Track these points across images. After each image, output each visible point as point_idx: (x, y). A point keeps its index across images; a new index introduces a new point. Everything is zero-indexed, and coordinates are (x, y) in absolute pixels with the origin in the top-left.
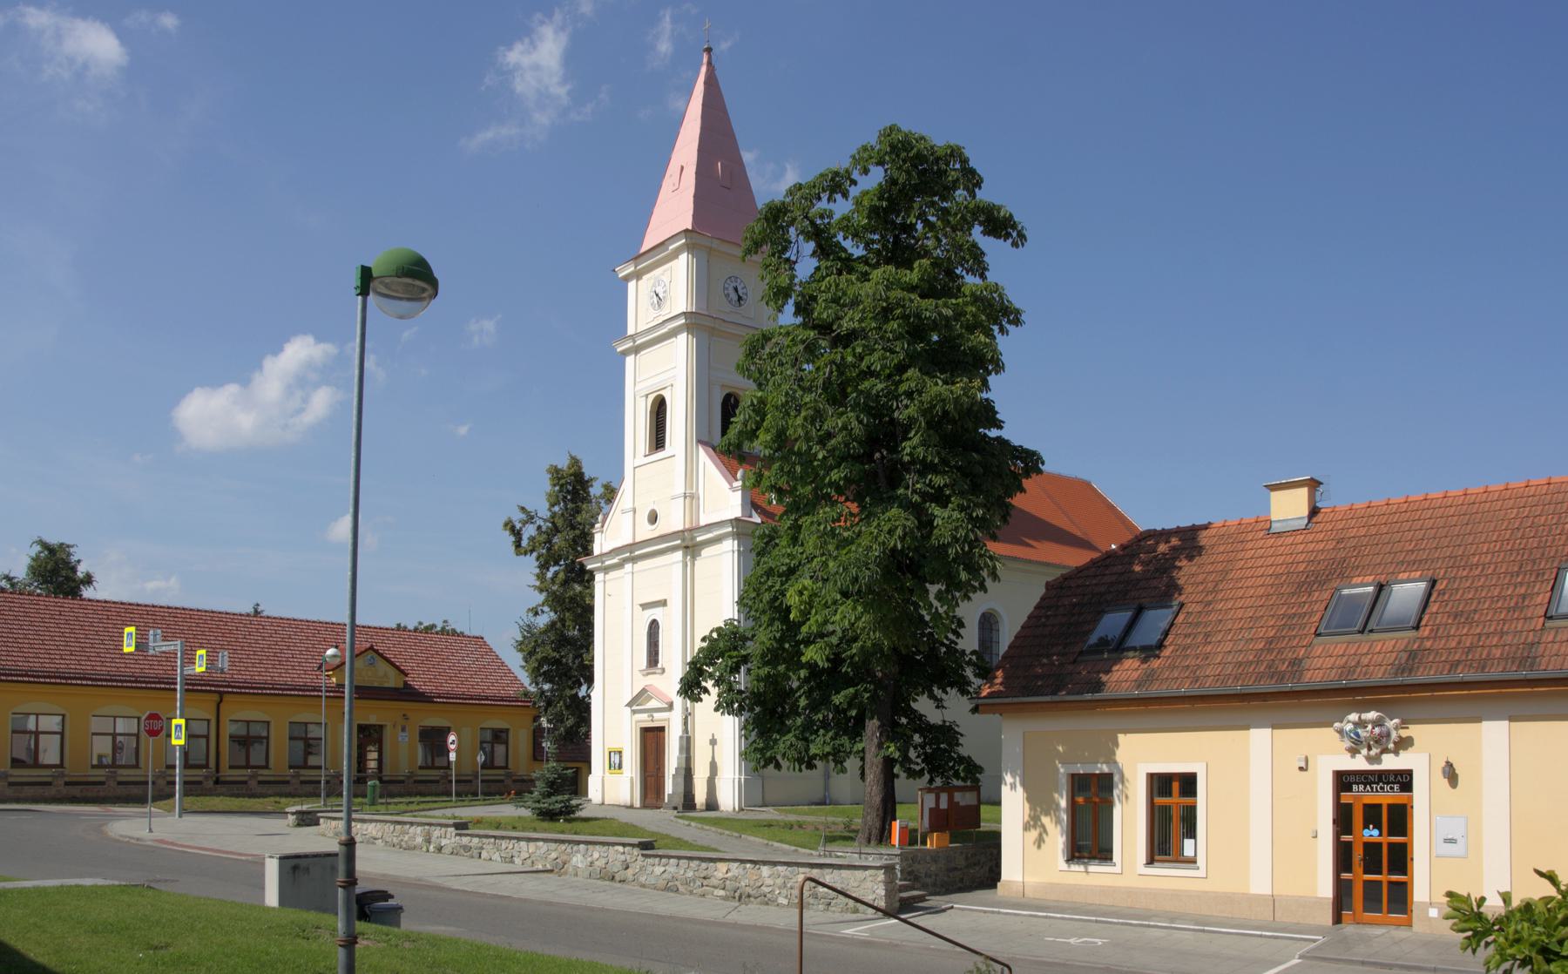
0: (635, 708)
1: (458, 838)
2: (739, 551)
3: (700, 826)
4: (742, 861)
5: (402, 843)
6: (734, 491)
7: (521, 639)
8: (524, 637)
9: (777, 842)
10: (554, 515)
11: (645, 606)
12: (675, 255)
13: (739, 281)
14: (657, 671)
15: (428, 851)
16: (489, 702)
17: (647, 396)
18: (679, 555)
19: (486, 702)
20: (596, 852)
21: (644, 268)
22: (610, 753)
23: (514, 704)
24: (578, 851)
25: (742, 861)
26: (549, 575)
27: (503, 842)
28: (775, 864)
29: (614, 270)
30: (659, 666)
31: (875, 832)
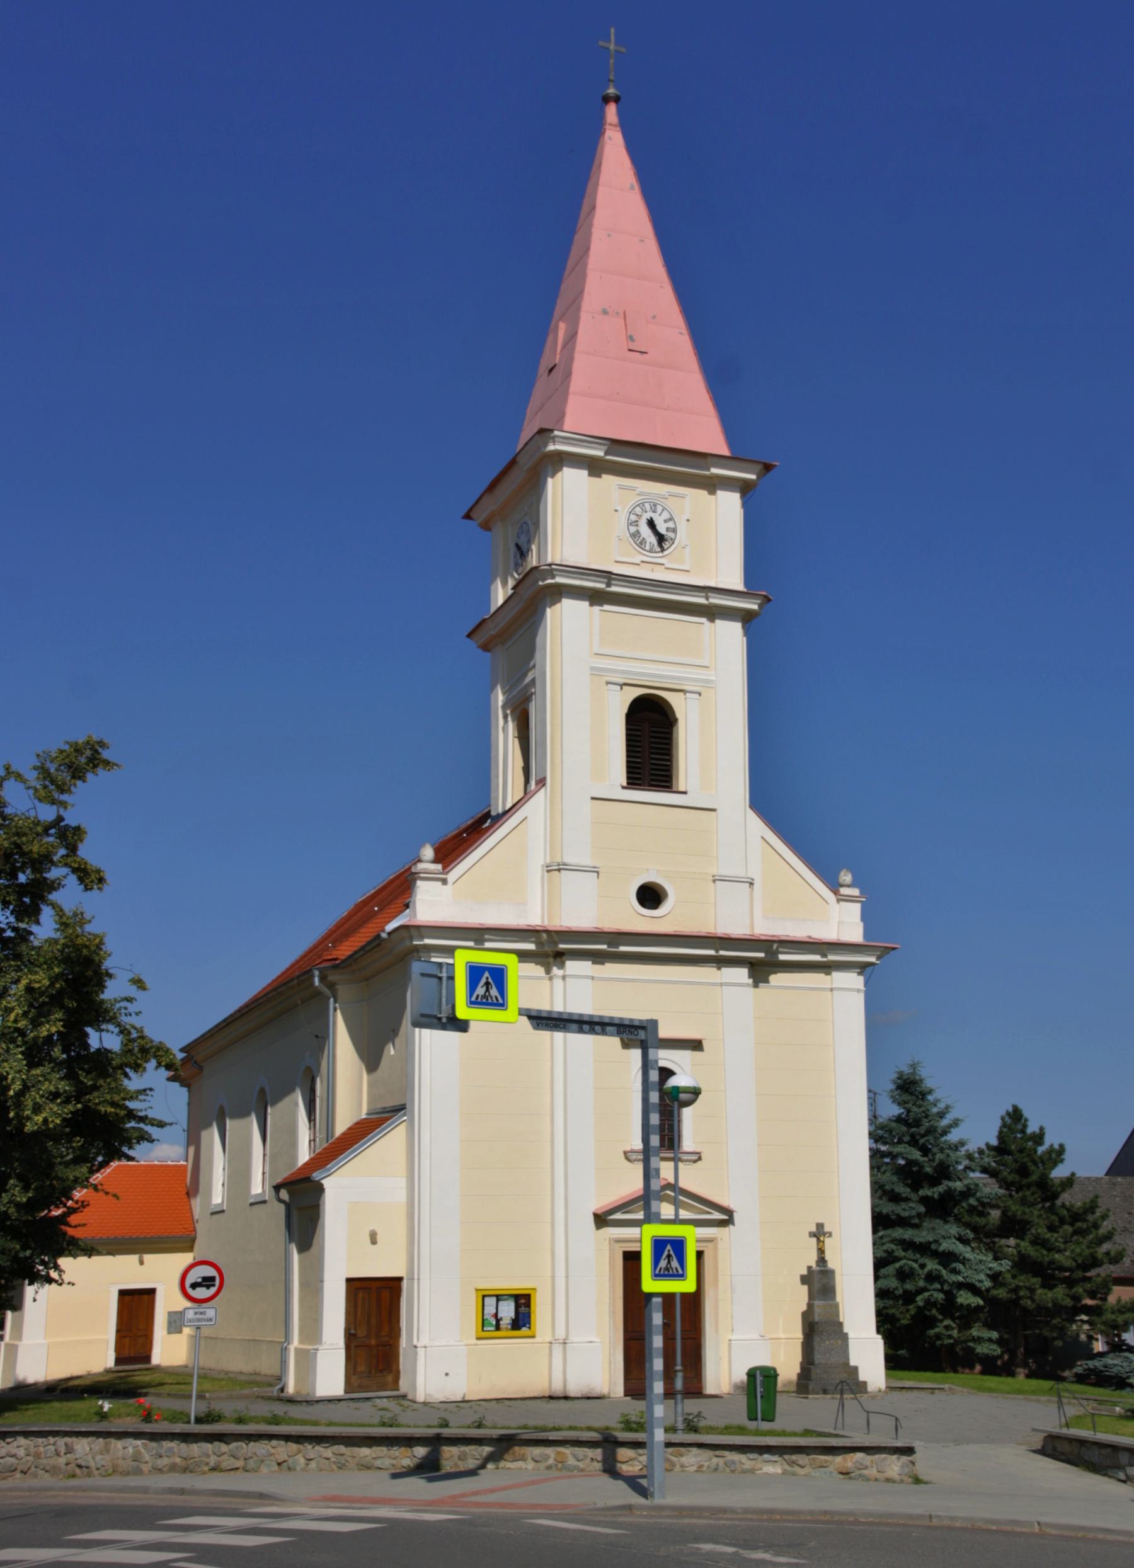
13: (659, 509)
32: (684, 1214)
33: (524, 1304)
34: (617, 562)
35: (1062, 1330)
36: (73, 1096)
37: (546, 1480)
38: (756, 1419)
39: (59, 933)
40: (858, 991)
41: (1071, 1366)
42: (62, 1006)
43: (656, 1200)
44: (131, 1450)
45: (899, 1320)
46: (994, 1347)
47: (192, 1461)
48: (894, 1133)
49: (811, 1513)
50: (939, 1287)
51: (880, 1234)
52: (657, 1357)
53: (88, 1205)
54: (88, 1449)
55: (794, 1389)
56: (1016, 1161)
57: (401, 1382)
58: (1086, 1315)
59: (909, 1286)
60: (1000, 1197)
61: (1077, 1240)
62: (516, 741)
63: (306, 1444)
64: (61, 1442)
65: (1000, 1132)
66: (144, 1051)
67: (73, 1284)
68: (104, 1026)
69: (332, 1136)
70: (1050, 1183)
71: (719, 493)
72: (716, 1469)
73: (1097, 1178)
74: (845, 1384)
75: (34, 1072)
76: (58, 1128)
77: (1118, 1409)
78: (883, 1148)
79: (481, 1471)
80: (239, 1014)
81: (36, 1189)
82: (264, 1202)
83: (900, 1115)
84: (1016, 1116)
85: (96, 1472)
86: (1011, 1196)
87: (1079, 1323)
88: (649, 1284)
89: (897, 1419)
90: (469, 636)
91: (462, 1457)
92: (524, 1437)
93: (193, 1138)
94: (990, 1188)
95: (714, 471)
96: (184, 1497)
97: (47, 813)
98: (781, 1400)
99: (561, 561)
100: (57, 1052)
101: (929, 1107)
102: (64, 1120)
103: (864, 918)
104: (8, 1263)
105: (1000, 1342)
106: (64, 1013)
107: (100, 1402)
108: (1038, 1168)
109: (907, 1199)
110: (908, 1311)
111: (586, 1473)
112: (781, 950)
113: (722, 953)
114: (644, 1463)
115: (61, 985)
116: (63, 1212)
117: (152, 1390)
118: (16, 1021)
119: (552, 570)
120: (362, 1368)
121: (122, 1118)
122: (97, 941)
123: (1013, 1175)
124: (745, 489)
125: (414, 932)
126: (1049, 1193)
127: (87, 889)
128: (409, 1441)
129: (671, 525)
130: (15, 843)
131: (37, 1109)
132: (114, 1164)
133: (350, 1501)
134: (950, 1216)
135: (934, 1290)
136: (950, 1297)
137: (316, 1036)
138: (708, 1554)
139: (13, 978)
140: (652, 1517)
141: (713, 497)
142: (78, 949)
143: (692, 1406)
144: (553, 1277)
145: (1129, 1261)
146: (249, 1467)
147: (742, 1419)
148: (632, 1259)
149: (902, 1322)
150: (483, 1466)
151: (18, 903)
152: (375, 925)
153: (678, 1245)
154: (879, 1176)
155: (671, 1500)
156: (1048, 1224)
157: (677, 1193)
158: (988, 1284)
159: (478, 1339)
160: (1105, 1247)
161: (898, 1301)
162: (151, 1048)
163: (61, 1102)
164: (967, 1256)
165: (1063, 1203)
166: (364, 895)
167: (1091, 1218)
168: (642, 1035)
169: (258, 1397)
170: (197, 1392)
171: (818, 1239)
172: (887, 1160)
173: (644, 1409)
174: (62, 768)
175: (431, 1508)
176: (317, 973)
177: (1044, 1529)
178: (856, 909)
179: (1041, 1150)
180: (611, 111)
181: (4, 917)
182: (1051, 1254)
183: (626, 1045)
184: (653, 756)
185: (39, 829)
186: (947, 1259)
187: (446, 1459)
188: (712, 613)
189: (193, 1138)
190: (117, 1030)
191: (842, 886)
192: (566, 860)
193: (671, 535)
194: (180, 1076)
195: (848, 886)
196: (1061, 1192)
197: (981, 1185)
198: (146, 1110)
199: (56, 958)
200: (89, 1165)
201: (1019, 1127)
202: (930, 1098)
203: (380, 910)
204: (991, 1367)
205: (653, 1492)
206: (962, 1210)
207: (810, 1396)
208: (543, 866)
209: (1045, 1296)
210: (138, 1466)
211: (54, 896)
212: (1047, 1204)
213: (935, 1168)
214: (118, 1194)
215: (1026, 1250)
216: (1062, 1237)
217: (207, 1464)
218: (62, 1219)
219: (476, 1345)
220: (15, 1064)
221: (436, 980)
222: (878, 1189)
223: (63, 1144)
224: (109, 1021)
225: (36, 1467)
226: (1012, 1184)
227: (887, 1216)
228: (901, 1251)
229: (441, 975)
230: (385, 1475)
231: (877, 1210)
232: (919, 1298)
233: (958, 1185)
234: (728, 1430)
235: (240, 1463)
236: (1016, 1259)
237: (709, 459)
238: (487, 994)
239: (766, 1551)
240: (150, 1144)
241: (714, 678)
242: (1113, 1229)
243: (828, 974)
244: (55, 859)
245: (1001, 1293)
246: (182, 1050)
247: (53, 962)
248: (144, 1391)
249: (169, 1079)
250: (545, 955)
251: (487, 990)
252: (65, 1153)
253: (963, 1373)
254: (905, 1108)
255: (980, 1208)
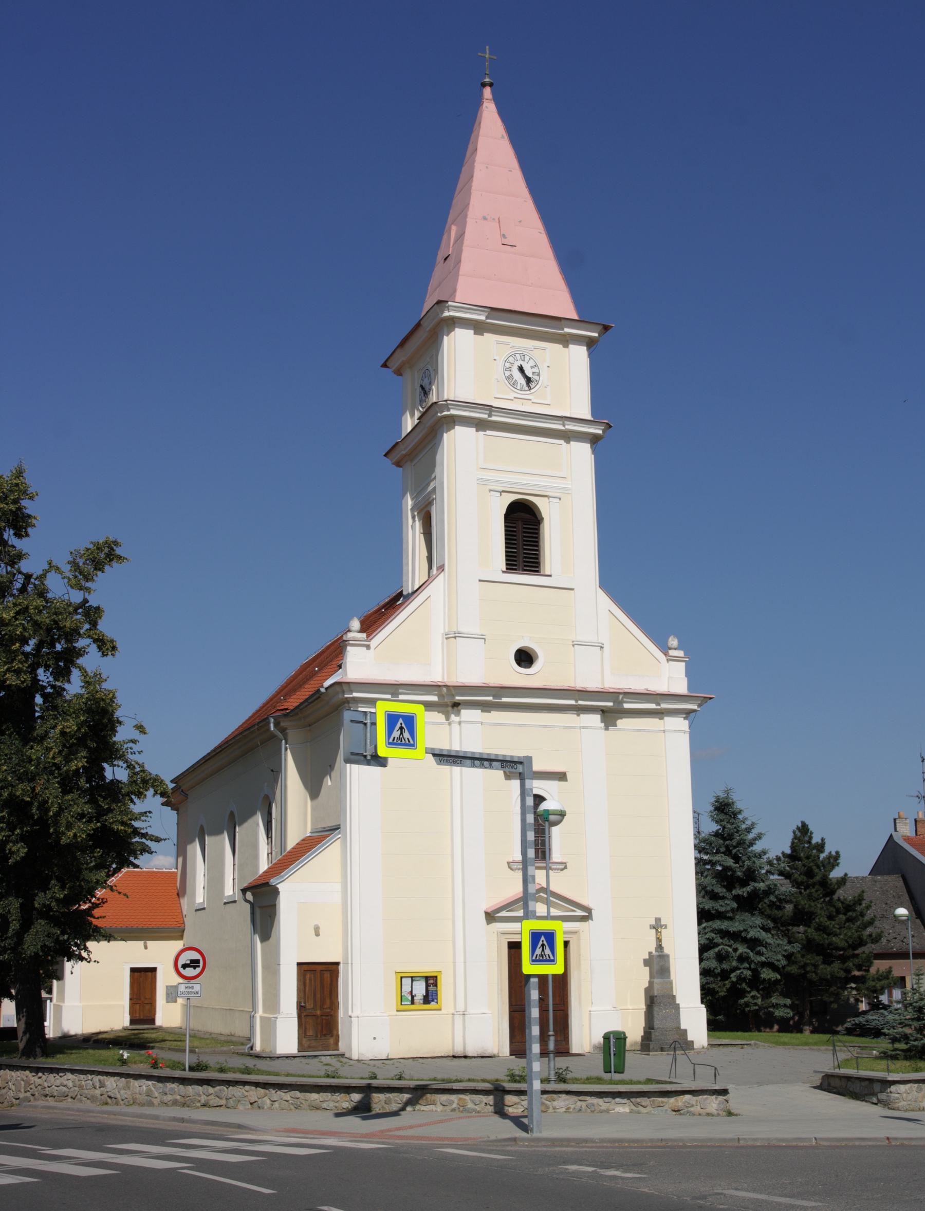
13: (527, 358)
32: (554, 912)
33: (432, 984)
34: (495, 398)
35: (837, 995)
36: (94, 817)
37: (451, 1119)
38: (610, 1072)
39: (84, 690)
40: (685, 732)
41: (843, 1023)
42: (86, 747)
43: (532, 900)
44: (144, 1088)
45: (718, 992)
46: (788, 1010)
47: (188, 1098)
48: (713, 845)
49: (651, 1140)
50: (748, 966)
51: (704, 925)
52: (535, 1025)
53: (106, 902)
54: (115, 1085)
55: (639, 1048)
56: (804, 865)
57: (340, 1044)
58: (854, 983)
59: (725, 966)
60: (793, 894)
61: (848, 926)
62: (422, 535)
63: (271, 1090)
64: (97, 1079)
65: (793, 843)
66: (145, 781)
67: (98, 962)
68: (116, 763)
69: (285, 851)
70: (829, 882)
71: (571, 346)
72: (580, 1110)
73: (863, 877)
74: (677, 1043)
75: (66, 798)
76: (84, 842)
77: (874, 1052)
78: (705, 857)
79: (402, 1113)
80: (214, 753)
81: (70, 888)
82: (235, 902)
83: (717, 831)
84: (804, 830)
85: (122, 1102)
86: (801, 893)
87: (849, 990)
88: (528, 968)
89: (715, 1068)
90: (385, 455)
91: (387, 1102)
92: (434, 1087)
93: (181, 851)
94: (785, 887)
95: (567, 330)
96: (184, 1124)
97: (76, 597)
98: (630, 1058)
99: (455, 397)
100: (82, 782)
101: (739, 824)
102: (88, 835)
103: (688, 674)
104: (53, 944)
105: (792, 1007)
106: (88, 751)
107: (121, 1052)
108: (820, 870)
109: (723, 898)
110: (724, 985)
111: (482, 1114)
112: (625, 700)
113: (580, 702)
114: (525, 1107)
115: (85, 730)
116: (89, 907)
117: (157, 1045)
118: (54, 758)
119: (448, 405)
120: (310, 1033)
121: (129, 834)
122: (111, 695)
123: (802, 877)
124: (590, 343)
125: (345, 687)
126: (829, 890)
127: (104, 655)
128: (348, 1089)
129: (535, 370)
130: (54, 621)
131: (69, 826)
132: (124, 870)
133: (305, 1132)
134: (756, 910)
135: (744, 968)
136: (755, 973)
137: (272, 771)
138: (574, 1172)
139: (51, 724)
140: (532, 1146)
141: (566, 349)
142: (97, 701)
143: (562, 1062)
144: (454, 962)
145: (885, 941)
146: (229, 1105)
147: (600, 1072)
148: (514, 947)
149: (720, 994)
150: (403, 1109)
151: (56, 666)
152: (316, 682)
153: (550, 937)
154: (703, 880)
155: (545, 1134)
156: (828, 914)
157: (548, 895)
158: (784, 962)
159: (398, 1011)
160: (869, 930)
161: (717, 978)
162: (150, 779)
163: (86, 821)
164: (768, 941)
165: (839, 898)
166: (308, 658)
167: (858, 908)
168: (520, 768)
169: (234, 1053)
170: (189, 1047)
171: (657, 930)
172: (708, 867)
173: (525, 1065)
174: (88, 562)
175: (365, 1140)
176: (272, 720)
177: (819, 1142)
178: (682, 666)
179: (822, 856)
180: (487, 92)
181: (46, 677)
182: (830, 937)
183: (508, 777)
184: (525, 547)
185: (71, 609)
186: (754, 943)
187: (376, 1103)
188: (568, 436)
189: (181, 851)
190: (125, 765)
191: (670, 649)
192: (461, 630)
193: (536, 377)
194: (171, 801)
195: (675, 649)
196: (837, 889)
197: (778, 885)
198: (146, 828)
199: (82, 709)
200: (106, 870)
201: (807, 838)
202: (740, 817)
203: (320, 670)
204: (786, 1027)
205: (532, 1129)
206: (764, 905)
207: (651, 1053)
208: (443, 634)
209: (826, 970)
210: (150, 1100)
211: (80, 661)
212: (827, 899)
213: (744, 872)
214: (128, 894)
215: (811, 935)
216: (838, 924)
217: (199, 1101)
218: (88, 912)
219: (396, 1016)
220: (53, 791)
221: (362, 725)
222: (703, 891)
223: (88, 854)
224: (119, 758)
225: (81, 1095)
226: (802, 883)
227: (709, 911)
228: (719, 938)
229: (366, 722)
230: (330, 1114)
231: (701, 906)
232: (732, 975)
233: (761, 886)
234: (589, 1080)
235: (223, 1102)
236: (805, 942)
237: (563, 321)
238: (401, 736)
239: (617, 1170)
240: (150, 855)
241: (570, 487)
242: (875, 916)
243: (661, 719)
244: (82, 632)
245: (793, 969)
246: (172, 781)
247: (79, 712)
248: (151, 1045)
249: (163, 804)
250: (446, 705)
251: (401, 733)
252: (89, 861)
253: (765, 1032)
254: (721, 825)
255: (778, 904)
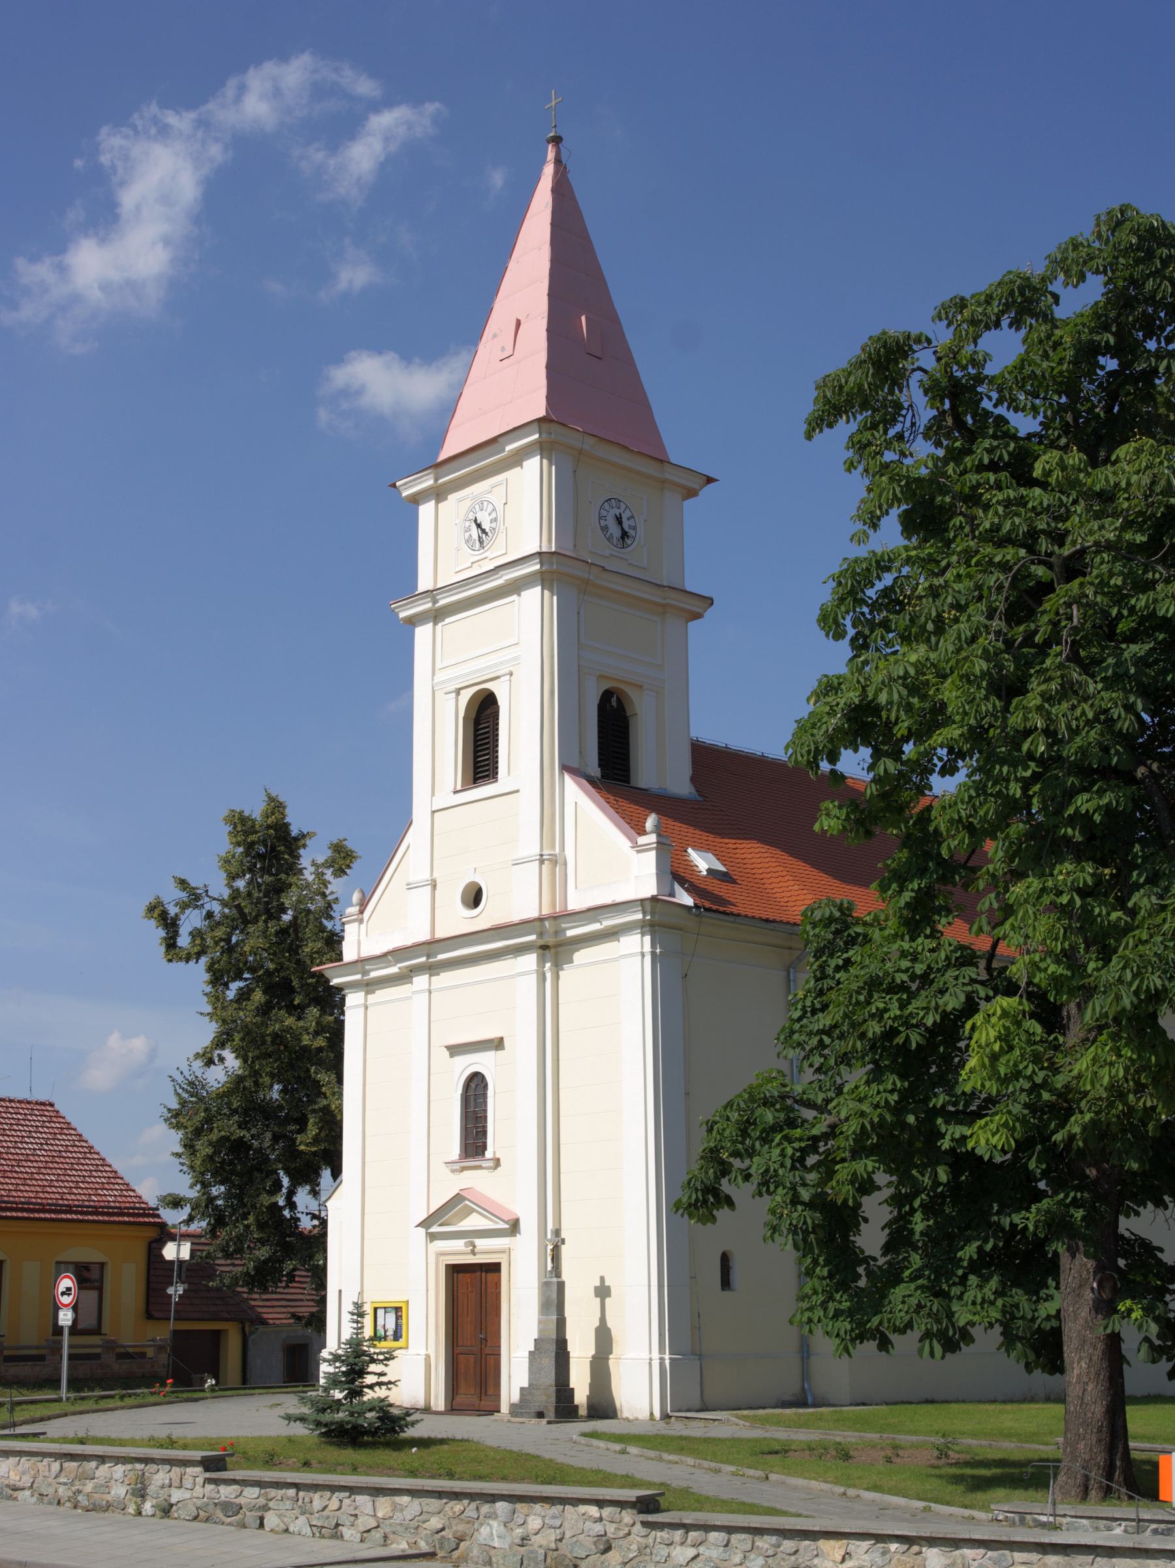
0: (432, 1230)
1: (210, 1487)
2: (653, 954)
3: (652, 1453)
4: (879, 1538)
5: (80, 1498)
6: (638, 852)
7: (177, 1106)
8: (183, 1103)
9: (867, 1489)
10: (236, 893)
11: (455, 1050)
12: (517, 459)
13: (623, 506)
14: (484, 1164)
15: (139, 1513)
16: (74, 1216)
17: (458, 692)
18: (530, 961)
19: (69, 1216)
20: (535, 1518)
21: (450, 481)
22: (376, 1309)
23: (116, 1219)
24: (492, 1516)
25: (879, 1538)
26: (231, 994)
27: (316, 1497)
28: (956, 1543)
29: (394, 485)
30: (489, 1154)
31: (1096, 1475)
